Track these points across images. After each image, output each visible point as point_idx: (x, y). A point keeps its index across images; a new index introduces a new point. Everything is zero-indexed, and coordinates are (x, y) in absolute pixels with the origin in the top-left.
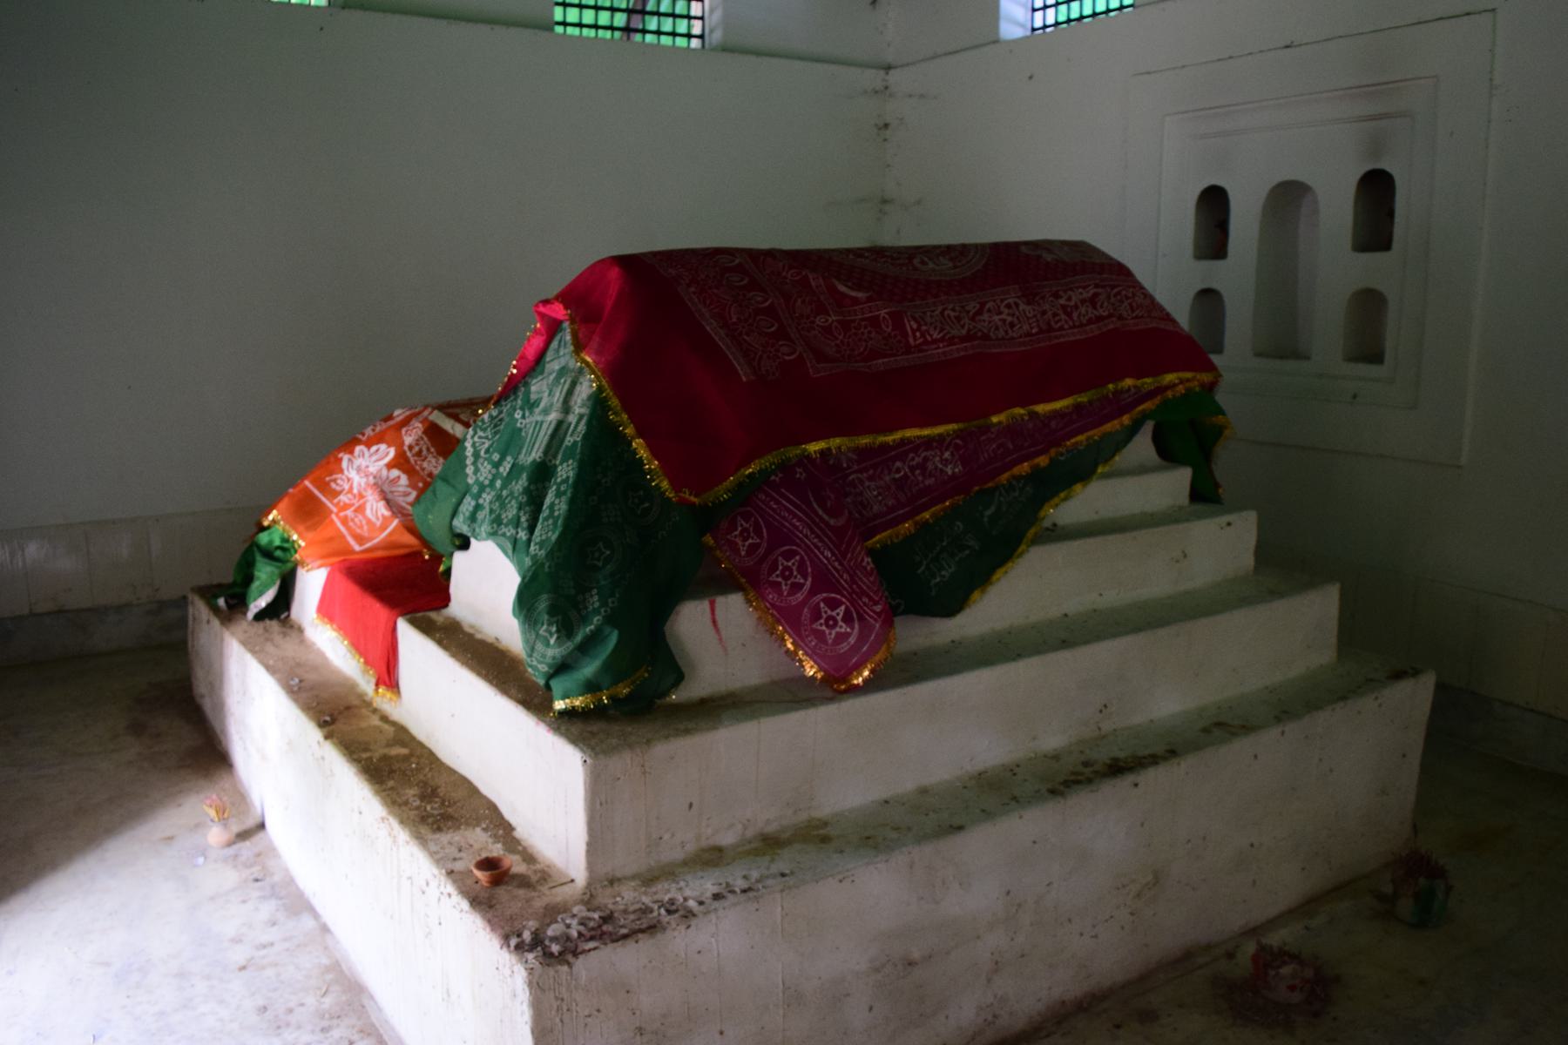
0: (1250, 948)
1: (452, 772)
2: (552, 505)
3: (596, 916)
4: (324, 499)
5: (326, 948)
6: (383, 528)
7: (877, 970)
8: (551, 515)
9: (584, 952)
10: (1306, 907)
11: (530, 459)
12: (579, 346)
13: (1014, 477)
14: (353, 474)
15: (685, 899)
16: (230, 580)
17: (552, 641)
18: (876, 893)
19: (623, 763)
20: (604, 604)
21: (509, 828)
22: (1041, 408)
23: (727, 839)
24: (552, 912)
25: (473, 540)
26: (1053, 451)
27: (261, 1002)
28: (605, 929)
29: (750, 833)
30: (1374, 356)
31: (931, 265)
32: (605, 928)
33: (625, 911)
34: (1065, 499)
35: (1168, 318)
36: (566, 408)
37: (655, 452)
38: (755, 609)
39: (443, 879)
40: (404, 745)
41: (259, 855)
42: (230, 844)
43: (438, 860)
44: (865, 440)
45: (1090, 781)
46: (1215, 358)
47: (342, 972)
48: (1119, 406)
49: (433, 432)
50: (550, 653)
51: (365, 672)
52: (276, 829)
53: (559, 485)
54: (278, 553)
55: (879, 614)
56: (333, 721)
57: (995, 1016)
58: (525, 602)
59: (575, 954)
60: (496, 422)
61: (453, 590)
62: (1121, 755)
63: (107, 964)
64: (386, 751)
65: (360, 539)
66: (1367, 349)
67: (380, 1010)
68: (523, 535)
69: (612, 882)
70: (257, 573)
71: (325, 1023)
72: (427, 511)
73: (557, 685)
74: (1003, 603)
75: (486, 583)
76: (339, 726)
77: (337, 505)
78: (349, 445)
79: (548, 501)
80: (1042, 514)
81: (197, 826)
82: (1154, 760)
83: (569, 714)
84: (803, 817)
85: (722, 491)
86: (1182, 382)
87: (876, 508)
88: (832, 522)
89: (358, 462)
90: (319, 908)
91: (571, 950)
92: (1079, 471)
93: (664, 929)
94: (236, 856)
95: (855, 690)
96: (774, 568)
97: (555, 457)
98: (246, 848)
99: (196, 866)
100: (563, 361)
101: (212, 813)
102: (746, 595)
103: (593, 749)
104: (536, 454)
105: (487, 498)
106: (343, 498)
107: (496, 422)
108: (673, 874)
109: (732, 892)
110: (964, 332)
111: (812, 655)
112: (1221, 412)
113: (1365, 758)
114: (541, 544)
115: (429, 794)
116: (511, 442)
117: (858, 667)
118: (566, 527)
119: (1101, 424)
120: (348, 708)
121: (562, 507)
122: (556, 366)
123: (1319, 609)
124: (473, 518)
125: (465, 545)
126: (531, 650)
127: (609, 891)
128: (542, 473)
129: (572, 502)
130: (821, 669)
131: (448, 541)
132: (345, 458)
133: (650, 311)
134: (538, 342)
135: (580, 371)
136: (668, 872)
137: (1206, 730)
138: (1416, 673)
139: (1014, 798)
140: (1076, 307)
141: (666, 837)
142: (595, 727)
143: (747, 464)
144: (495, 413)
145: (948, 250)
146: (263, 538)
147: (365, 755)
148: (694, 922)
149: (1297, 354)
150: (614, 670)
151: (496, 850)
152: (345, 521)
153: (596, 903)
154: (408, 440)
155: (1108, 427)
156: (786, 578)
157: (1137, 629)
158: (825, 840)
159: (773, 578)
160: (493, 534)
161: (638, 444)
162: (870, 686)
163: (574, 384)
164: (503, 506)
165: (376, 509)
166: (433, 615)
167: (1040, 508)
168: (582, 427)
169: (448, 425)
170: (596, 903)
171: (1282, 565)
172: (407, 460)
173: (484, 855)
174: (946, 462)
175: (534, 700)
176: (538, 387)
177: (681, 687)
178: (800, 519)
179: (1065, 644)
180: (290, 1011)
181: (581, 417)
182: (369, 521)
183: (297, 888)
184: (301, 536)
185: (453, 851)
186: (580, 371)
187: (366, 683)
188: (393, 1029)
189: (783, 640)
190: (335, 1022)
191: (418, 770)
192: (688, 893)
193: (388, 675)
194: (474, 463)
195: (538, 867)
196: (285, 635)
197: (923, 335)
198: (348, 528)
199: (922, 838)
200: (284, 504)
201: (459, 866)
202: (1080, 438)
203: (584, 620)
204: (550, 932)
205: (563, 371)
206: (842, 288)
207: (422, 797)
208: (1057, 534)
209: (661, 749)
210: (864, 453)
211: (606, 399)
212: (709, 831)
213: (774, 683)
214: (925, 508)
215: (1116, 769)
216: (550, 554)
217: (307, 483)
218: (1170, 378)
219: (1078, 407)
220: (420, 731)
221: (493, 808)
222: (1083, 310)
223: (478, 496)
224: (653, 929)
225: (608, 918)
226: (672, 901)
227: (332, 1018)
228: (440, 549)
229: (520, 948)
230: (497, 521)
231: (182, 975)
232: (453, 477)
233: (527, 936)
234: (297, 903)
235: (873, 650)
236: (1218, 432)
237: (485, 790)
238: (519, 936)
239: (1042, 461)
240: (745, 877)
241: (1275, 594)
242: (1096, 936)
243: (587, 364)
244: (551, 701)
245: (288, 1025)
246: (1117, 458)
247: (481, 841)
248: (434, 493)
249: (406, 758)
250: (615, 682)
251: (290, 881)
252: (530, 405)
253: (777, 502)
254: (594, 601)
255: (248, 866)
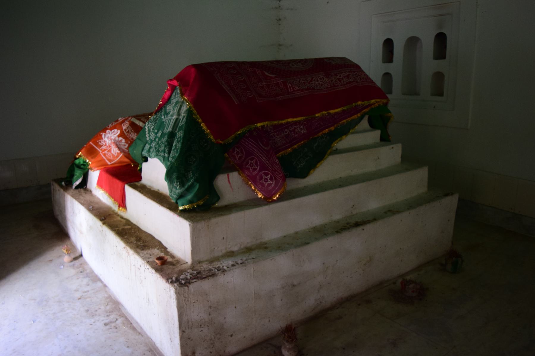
0: (400, 280)
1: (165, 207)
2: (176, 145)
3: (195, 272)
4: (97, 148)
5: (106, 292)
6: (118, 157)
7: (283, 288)
8: (176, 148)
9: (192, 282)
10: (419, 268)
11: (168, 131)
12: (182, 94)
13: (323, 134)
14: (106, 139)
15: (223, 266)
16: (65, 177)
17: (178, 188)
18: (283, 264)
19: (202, 225)
20: (194, 175)
21: (165, 248)
22: (332, 111)
23: (235, 249)
24: (181, 272)
25: (149, 158)
26: (335, 125)
27: (86, 309)
28: (198, 276)
29: (242, 247)
30: (441, 94)
31: (295, 66)
32: (198, 276)
33: (204, 271)
34: (340, 141)
35: (372, 82)
36: (179, 114)
37: (208, 128)
38: (242, 176)
39: (146, 264)
40: (129, 225)
41: (81, 264)
42: (71, 261)
43: (144, 258)
44: (275, 122)
45: (349, 229)
46: (388, 96)
47: (112, 298)
48: (357, 110)
49: (132, 124)
50: (177, 191)
51: (114, 203)
52: (87, 256)
53: (178, 139)
54: (82, 166)
55: (281, 177)
56: (105, 219)
57: (321, 302)
58: (169, 176)
59: (190, 283)
60: (155, 120)
61: (143, 175)
62: (359, 221)
63: (35, 300)
64: (123, 227)
65: (110, 161)
66: (438, 91)
67: (125, 309)
68: (166, 155)
69: (200, 262)
70: (75, 173)
71: (108, 314)
72: (133, 150)
73: (180, 202)
74: (321, 173)
75: (155, 172)
76: (107, 220)
77: (101, 150)
78: (104, 130)
79: (174, 144)
80: (333, 145)
81: (60, 256)
82: (369, 222)
83: (184, 211)
84: (259, 241)
85: (230, 139)
86: (377, 102)
87: (279, 144)
88: (266, 148)
89: (108, 135)
90: (103, 280)
91: (188, 283)
92: (344, 132)
93: (217, 275)
94: (74, 265)
95: (274, 201)
96: (247, 163)
97: (176, 130)
98: (77, 262)
99: (61, 269)
100: (177, 99)
101: (65, 251)
102: (239, 172)
103: (192, 221)
104: (170, 129)
105: (153, 144)
106: (103, 147)
107: (155, 120)
108: (219, 259)
109: (237, 264)
110: (306, 87)
111: (260, 191)
112: (390, 112)
113: (436, 221)
114: (173, 158)
115: (139, 239)
116: (161, 126)
117: (275, 194)
118: (181, 151)
119: (351, 116)
120: (109, 215)
121: (179, 145)
122: (175, 101)
123: (421, 175)
124: (149, 151)
125: (146, 160)
126: (171, 191)
127: (199, 265)
128: (172, 135)
129: (183, 144)
130: (263, 195)
131: (141, 159)
132: (104, 134)
133: (205, 82)
134: (168, 93)
135: (183, 102)
136: (217, 259)
137: (385, 213)
138: (452, 194)
139: (325, 234)
140: (342, 79)
141: (216, 248)
142: (192, 214)
143: (238, 131)
144: (155, 117)
145: (301, 61)
146: (77, 162)
147: (117, 229)
148: (226, 273)
149: (416, 94)
150: (198, 197)
151: (162, 255)
152: (105, 155)
153: (195, 269)
154: (124, 128)
155: (353, 117)
156: (251, 167)
157: (364, 181)
158: (266, 248)
159: (247, 166)
160: (157, 155)
161: (202, 125)
162: (279, 200)
163: (181, 106)
164: (160, 146)
165: (115, 150)
166: (137, 183)
167: (332, 143)
168: (185, 120)
169: (137, 122)
170: (195, 269)
171: (409, 161)
172: (124, 134)
173: (158, 256)
174: (301, 129)
175: (172, 207)
176: (169, 108)
177: (220, 201)
178: (255, 148)
179: (340, 186)
180: (96, 311)
181: (184, 117)
182: (113, 155)
183: (95, 274)
184: (90, 160)
185: (148, 256)
186: (183, 102)
187: (115, 207)
188: (130, 314)
189: (251, 186)
190: (111, 313)
191: (135, 232)
192: (223, 265)
193: (122, 203)
194: (149, 133)
195: (176, 259)
196: (86, 193)
197: (293, 88)
198: (106, 157)
199: (297, 246)
200: (83, 150)
201: (150, 260)
202: (345, 121)
203: (188, 181)
204: (181, 277)
205: (177, 102)
206: (267, 74)
207: (137, 240)
208: (337, 152)
209: (214, 221)
210: (275, 127)
211: (192, 111)
212: (230, 246)
213: (248, 200)
214: (295, 144)
215: (357, 225)
216: (176, 160)
217: (91, 143)
218: (373, 101)
219: (343, 111)
220: (134, 221)
221: (160, 243)
222: (345, 80)
223: (150, 144)
224: (213, 275)
225: (199, 273)
226: (219, 267)
227: (110, 312)
228: (138, 161)
229: (172, 282)
230: (158, 151)
231: (60, 302)
232: (142, 138)
233: (174, 279)
234: (96, 279)
235: (279, 189)
236: (389, 118)
237: (157, 237)
238: (171, 279)
239: (332, 128)
240: (241, 260)
241: (407, 170)
242: (352, 277)
243: (186, 100)
244: (178, 207)
245: (96, 315)
246: (356, 127)
247: (157, 252)
248: (136, 143)
249: (130, 229)
250: (199, 199)
251: (92, 272)
252: (167, 114)
253: (248, 143)
254: (191, 175)
255: (78, 268)
